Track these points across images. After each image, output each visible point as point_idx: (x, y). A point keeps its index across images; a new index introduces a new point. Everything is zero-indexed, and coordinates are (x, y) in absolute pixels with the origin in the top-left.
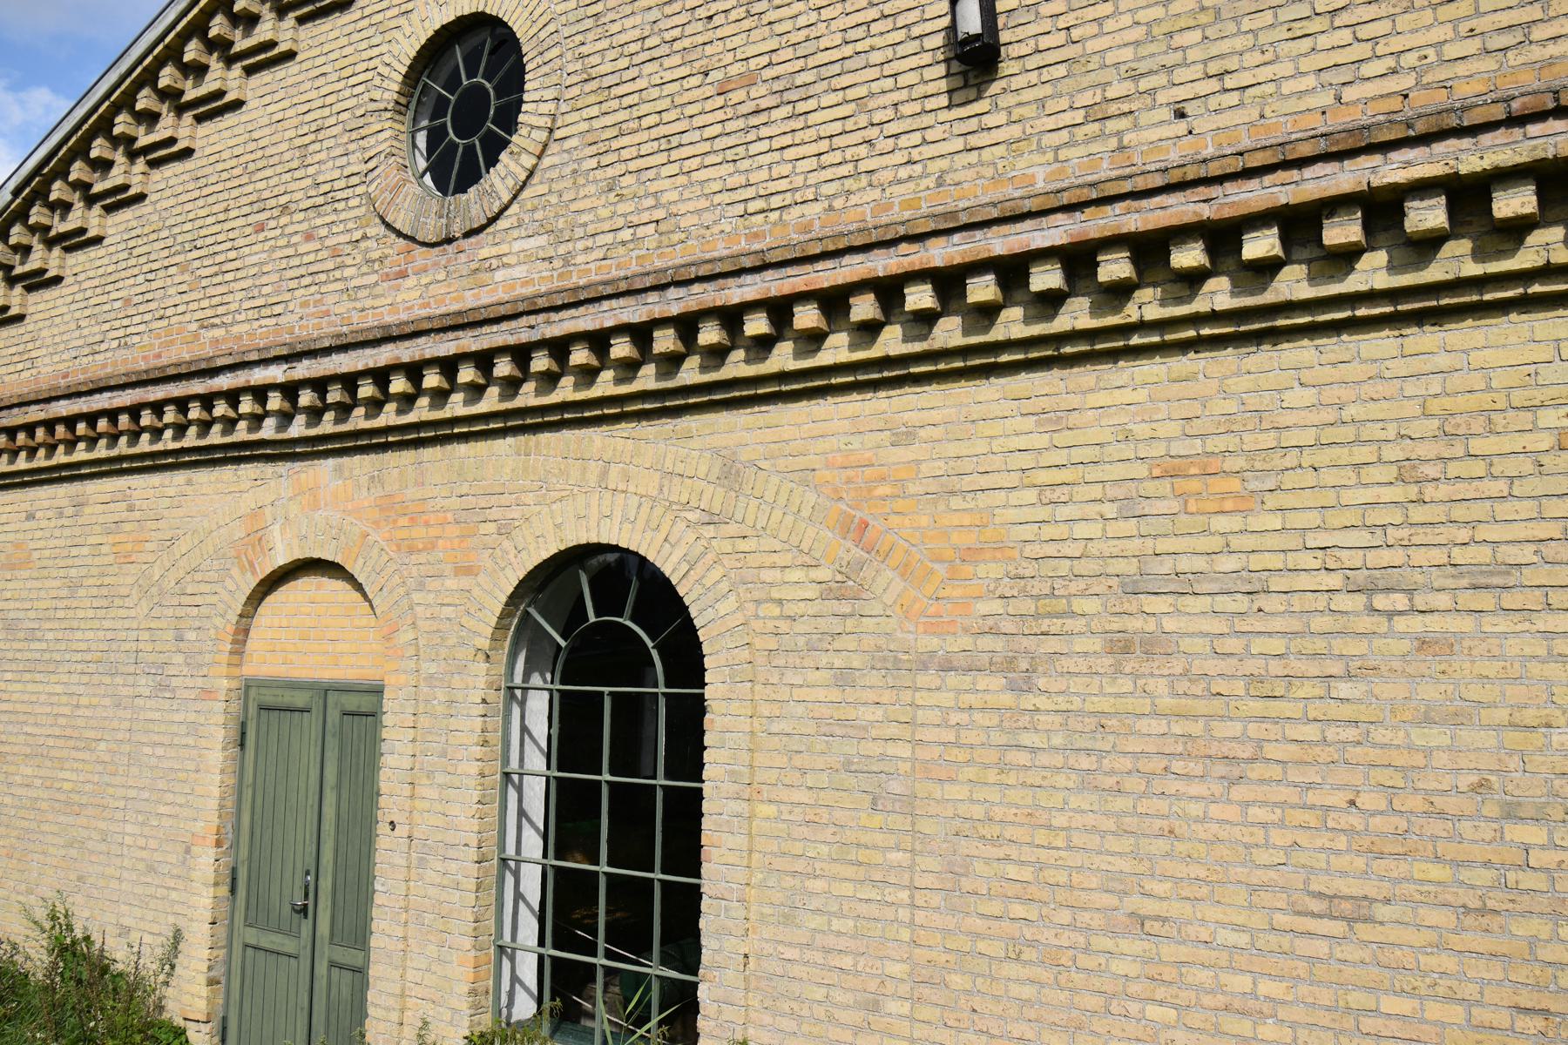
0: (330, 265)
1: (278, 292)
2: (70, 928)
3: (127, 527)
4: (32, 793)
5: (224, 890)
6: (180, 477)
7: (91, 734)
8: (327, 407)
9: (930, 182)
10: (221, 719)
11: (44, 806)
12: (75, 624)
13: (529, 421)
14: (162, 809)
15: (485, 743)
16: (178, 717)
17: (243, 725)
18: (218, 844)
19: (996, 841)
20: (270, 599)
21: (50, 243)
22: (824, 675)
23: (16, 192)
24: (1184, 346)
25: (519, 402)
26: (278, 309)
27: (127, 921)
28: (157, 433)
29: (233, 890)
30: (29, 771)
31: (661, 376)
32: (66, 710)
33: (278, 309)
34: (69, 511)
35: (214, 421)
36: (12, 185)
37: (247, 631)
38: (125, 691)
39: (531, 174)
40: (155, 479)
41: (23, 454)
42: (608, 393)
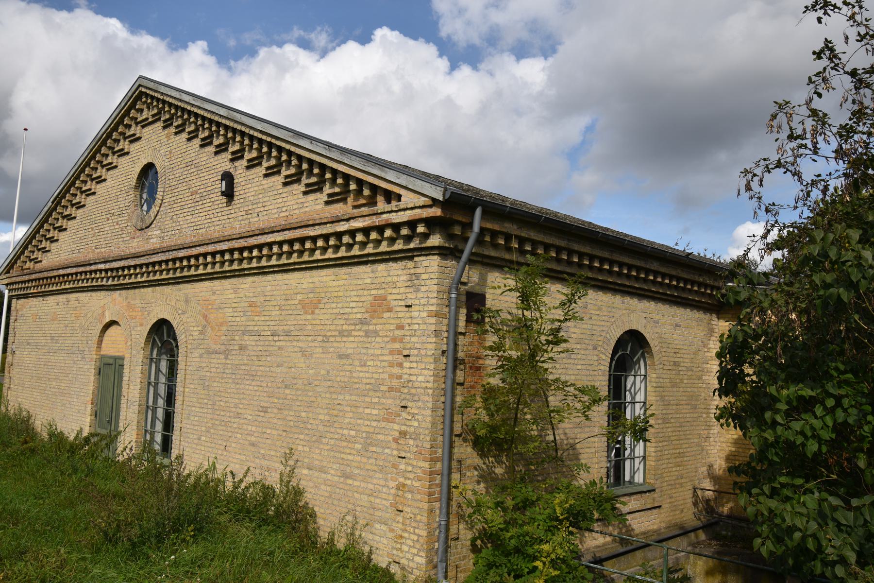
0: (120, 233)
1: (110, 240)
2: (56, 429)
3: (78, 309)
4: (55, 390)
5: (93, 417)
6: (89, 294)
7: (68, 372)
8: (294, 252)
9: (222, 226)
10: (93, 367)
11: (57, 394)
12: (66, 338)
13: (319, 264)
14: (82, 394)
15: (142, 373)
16: (86, 367)
17: (100, 369)
18: (92, 404)
19: (220, 396)
20: (107, 332)
21: (64, 217)
22: (197, 355)
23: (53, 202)
24: (255, 274)
25: (352, 253)
26: (110, 245)
27: (73, 428)
28: (197, 267)
29: (96, 417)
30: (54, 383)
31: (360, 249)
32: (63, 365)
33: (110, 245)
34: (66, 303)
35: (305, 250)
36: (51, 200)
37: (102, 341)
38: (76, 359)
39: (158, 212)
40: (84, 294)
41: (111, 279)
42: (357, 254)
